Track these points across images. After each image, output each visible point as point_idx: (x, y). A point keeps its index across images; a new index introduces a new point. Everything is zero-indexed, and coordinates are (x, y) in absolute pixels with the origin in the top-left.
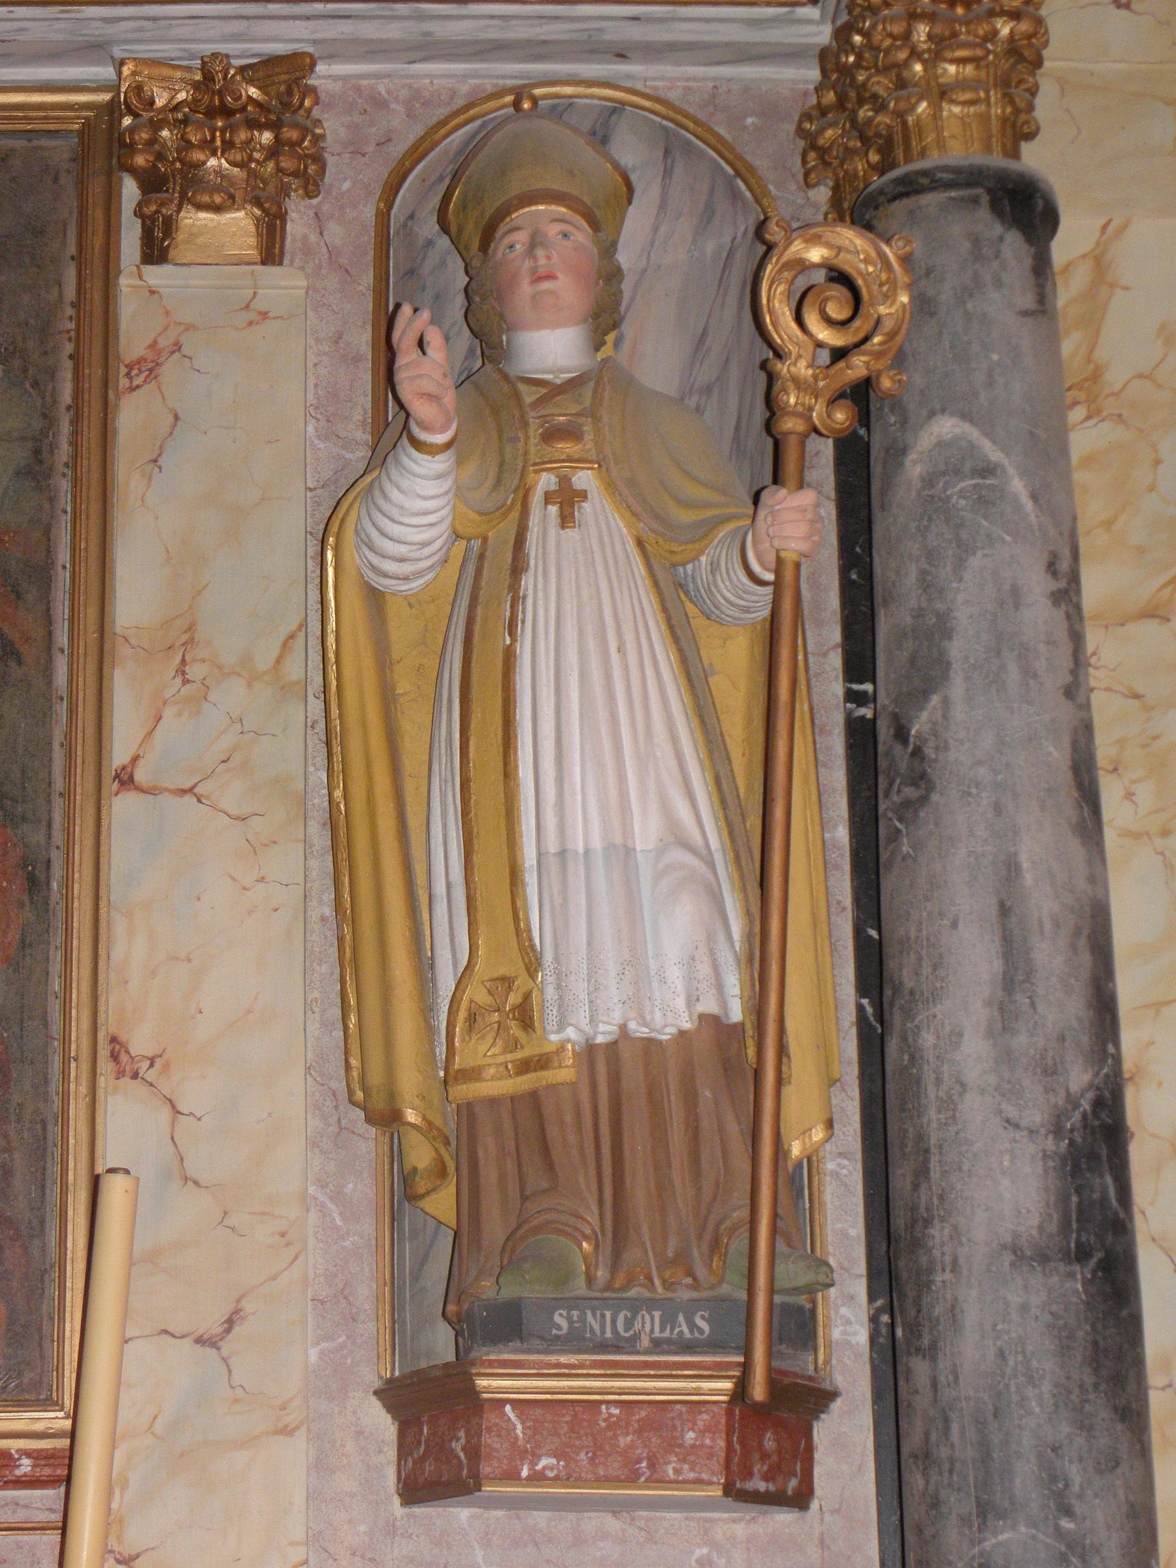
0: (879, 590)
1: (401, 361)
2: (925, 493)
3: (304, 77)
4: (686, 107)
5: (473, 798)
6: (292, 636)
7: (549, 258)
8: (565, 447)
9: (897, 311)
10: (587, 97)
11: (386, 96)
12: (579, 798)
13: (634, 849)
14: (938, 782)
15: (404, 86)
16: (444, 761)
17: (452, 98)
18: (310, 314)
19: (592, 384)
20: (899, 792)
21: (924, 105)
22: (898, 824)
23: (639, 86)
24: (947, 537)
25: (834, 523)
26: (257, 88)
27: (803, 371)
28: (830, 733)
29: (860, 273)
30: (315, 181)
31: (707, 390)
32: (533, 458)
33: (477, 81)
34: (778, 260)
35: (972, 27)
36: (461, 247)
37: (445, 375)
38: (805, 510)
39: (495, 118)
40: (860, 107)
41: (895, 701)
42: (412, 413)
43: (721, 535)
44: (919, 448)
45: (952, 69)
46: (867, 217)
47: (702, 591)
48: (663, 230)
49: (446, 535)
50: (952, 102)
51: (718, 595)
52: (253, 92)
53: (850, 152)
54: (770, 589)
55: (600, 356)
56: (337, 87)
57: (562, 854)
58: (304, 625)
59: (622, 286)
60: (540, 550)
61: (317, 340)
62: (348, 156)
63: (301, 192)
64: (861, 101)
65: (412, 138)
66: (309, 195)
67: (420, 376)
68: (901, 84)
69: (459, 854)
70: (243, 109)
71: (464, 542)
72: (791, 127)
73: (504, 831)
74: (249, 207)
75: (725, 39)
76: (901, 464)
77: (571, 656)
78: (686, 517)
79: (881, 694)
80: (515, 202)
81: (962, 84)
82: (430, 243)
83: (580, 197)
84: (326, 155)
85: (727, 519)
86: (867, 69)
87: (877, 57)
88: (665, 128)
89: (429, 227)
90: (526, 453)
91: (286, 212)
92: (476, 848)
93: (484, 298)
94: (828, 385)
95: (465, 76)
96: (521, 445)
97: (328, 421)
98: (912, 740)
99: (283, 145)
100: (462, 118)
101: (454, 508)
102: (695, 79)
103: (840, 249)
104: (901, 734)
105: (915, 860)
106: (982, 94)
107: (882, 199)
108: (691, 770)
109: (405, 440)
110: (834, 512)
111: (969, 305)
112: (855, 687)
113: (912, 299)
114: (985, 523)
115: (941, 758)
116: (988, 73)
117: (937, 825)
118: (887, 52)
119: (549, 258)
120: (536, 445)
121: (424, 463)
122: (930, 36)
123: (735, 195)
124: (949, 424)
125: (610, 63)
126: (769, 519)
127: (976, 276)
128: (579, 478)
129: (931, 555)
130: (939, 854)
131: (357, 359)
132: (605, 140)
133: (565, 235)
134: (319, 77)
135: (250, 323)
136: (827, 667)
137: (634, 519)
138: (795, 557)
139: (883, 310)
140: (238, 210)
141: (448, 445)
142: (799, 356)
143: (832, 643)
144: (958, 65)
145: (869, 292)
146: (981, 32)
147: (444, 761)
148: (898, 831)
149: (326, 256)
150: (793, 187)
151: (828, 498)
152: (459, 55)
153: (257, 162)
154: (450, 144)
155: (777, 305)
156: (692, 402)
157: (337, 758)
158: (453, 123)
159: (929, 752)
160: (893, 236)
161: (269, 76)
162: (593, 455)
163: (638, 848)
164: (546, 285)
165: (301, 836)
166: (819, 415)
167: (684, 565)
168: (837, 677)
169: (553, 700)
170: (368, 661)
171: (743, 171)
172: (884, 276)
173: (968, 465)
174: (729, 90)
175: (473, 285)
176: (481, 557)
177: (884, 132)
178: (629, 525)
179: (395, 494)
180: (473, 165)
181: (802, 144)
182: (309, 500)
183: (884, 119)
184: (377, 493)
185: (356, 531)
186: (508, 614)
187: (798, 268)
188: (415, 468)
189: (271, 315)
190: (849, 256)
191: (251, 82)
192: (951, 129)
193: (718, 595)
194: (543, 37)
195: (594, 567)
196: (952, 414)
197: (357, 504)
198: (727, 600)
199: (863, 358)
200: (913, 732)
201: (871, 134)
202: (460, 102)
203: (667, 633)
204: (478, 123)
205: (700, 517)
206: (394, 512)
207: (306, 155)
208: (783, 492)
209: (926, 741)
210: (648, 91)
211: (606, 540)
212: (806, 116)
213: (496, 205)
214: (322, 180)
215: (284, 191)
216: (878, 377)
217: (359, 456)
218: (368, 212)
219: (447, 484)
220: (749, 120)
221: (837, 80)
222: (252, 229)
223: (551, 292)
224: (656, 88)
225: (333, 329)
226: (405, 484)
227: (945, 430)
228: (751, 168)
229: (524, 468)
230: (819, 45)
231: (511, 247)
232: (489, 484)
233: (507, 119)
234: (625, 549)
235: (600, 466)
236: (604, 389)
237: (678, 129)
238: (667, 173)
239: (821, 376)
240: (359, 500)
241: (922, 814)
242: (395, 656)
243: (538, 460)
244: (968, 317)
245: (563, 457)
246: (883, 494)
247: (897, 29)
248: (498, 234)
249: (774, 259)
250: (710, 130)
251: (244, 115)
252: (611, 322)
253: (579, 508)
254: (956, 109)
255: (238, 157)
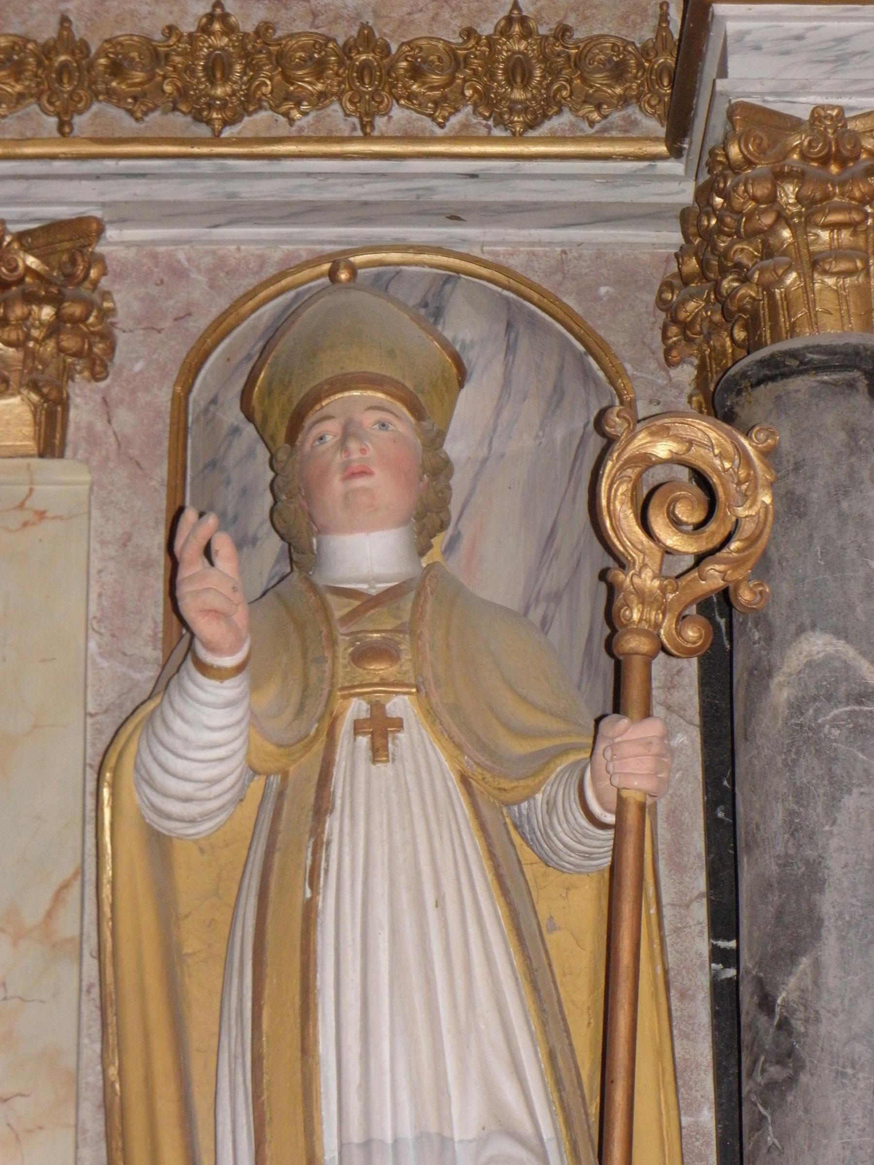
0: (741, 831)
1: (183, 573)
2: (793, 721)
3: (90, 245)
4: (530, 275)
5: (266, 1078)
6: (65, 886)
7: (363, 451)
8: (380, 669)
9: (758, 513)
10: (416, 264)
11: (186, 264)
12: (387, 1078)
13: (452, 1139)
14: (807, 1059)
15: (207, 252)
16: (234, 1034)
17: (261, 267)
18: (95, 513)
19: (412, 595)
20: (763, 1071)
21: (794, 275)
22: (761, 1109)
23: (476, 252)
24: (818, 772)
25: (699, 752)
26: (34, 255)
27: (649, 582)
28: (693, 998)
29: (715, 470)
30: (102, 361)
31: (556, 597)
32: (341, 682)
33: (291, 247)
34: (619, 455)
35: (848, 188)
36: (266, 438)
37: (234, 589)
38: (651, 743)
39: (310, 288)
40: (724, 277)
41: (759, 964)
42: (196, 632)
43: (558, 769)
44: (785, 669)
45: (825, 235)
46: (729, 403)
47: (538, 834)
48: (506, 414)
49: (239, 770)
50: (826, 272)
51: (554, 838)
52: (32, 261)
53: (715, 327)
54: (610, 834)
55: (424, 562)
56: (130, 254)
57: (367, 1144)
58: (81, 872)
59: (451, 482)
60: (348, 789)
61: (103, 543)
62: (142, 332)
63: (86, 374)
64: (723, 271)
65: (215, 311)
66: (96, 377)
67: (207, 590)
68: (768, 252)
69: (250, 1143)
70: (20, 281)
71: (264, 777)
72: (651, 298)
73: (300, 1118)
74: (25, 392)
75: (572, 198)
76: (767, 687)
77: (381, 910)
78: (519, 748)
79: (744, 955)
80: (326, 387)
81: (837, 253)
82: (235, 431)
83: (402, 381)
84: (117, 332)
85: (566, 750)
86: (729, 235)
87: (739, 221)
88: (507, 300)
89: (233, 415)
90: (333, 675)
91: (68, 397)
92: (268, 1137)
93: (291, 496)
94: (678, 598)
95: (277, 242)
96: (327, 666)
97: (113, 636)
98: (777, 1009)
99: (65, 322)
100: (272, 289)
101: (248, 740)
102: (540, 243)
103: (691, 442)
104: (766, 1003)
105: (781, 1153)
106: (859, 264)
107: (745, 383)
108: (520, 1044)
109: (189, 663)
110: (698, 740)
111: (845, 505)
112: (722, 944)
113: (774, 496)
114: (861, 755)
115: (812, 1030)
116: (867, 239)
117: (806, 1111)
118: (750, 216)
119: (363, 451)
120: (345, 666)
121: (210, 689)
122: (799, 199)
123: (586, 374)
124: (820, 642)
125: (444, 225)
126: (609, 754)
127: (852, 473)
128: (395, 704)
129: (800, 794)
130: (809, 1147)
131: (147, 565)
132: (438, 314)
133: (383, 425)
134: (110, 244)
135: (25, 524)
136: (689, 920)
137: (457, 752)
138: (639, 797)
139: (742, 512)
140: (12, 395)
141: (239, 669)
142: (644, 565)
143: (696, 893)
144: (832, 231)
145: (727, 493)
146: (857, 194)
147: (234, 1034)
148: (763, 1118)
149: (115, 446)
150: (653, 365)
151: (691, 723)
152: (266, 218)
153: (36, 340)
154: (259, 318)
155: (618, 506)
156: (536, 615)
157: (111, 1030)
158: (262, 295)
159: (798, 1026)
160: (753, 427)
161: (49, 244)
162: (411, 678)
163: (457, 1138)
164: (360, 482)
165: (72, 1121)
166: (668, 634)
167: (518, 803)
168: (701, 932)
169: (358, 963)
170: (148, 919)
171: (595, 348)
172: (742, 474)
173: (843, 689)
174: (580, 256)
175: (279, 480)
176: (281, 795)
177: (749, 307)
178: (452, 758)
179: (178, 725)
180: (281, 344)
181: (662, 316)
182: (89, 728)
183: (748, 291)
184: (158, 723)
185: (136, 768)
186: (309, 862)
187: (643, 465)
188: (201, 695)
189: (49, 514)
190: (702, 451)
191: (29, 250)
192: (826, 302)
193: (554, 838)
194: (364, 198)
195: (410, 807)
196: (824, 630)
197: (135, 738)
198: (565, 845)
199: (717, 567)
200: (779, 1001)
201: (733, 308)
202: (270, 271)
203: (494, 885)
204: (291, 294)
205: (534, 749)
206: (178, 745)
207: (92, 333)
208: (625, 722)
209: (795, 1011)
210: (486, 257)
211: (425, 775)
212: (667, 285)
213: (305, 391)
214: (111, 360)
215: (67, 373)
216: (736, 589)
217: (147, 676)
218: (163, 396)
219: (239, 713)
220: (603, 290)
221: (700, 245)
222: (28, 416)
223: (365, 490)
224: (496, 254)
225: (120, 531)
226: (189, 713)
227: (815, 649)
228: (603, 344)
229: (330, 693)
230: (681, 204)
231: (321, 439)
232: (288, 714)
233: (323, 289)
234: (447, 787)
235: (418, 691)
236: (426, 601)
237: (521, 300)
238: (510, 349)
239: (669, 587)
240: (139, 730)
241: (790, 1098)
242: (183, 909)
243: (347, 684)
244: (842, 517)
245: (376, 680)
246: (747, 720)
247: (761, 191)
248: (308, 422)
249: (615, 455)
250: (556, 300)
251: (21, 287)
252: (438, 523)
253: (394, 739)
254: (831, 281)
255: (13, 336)
